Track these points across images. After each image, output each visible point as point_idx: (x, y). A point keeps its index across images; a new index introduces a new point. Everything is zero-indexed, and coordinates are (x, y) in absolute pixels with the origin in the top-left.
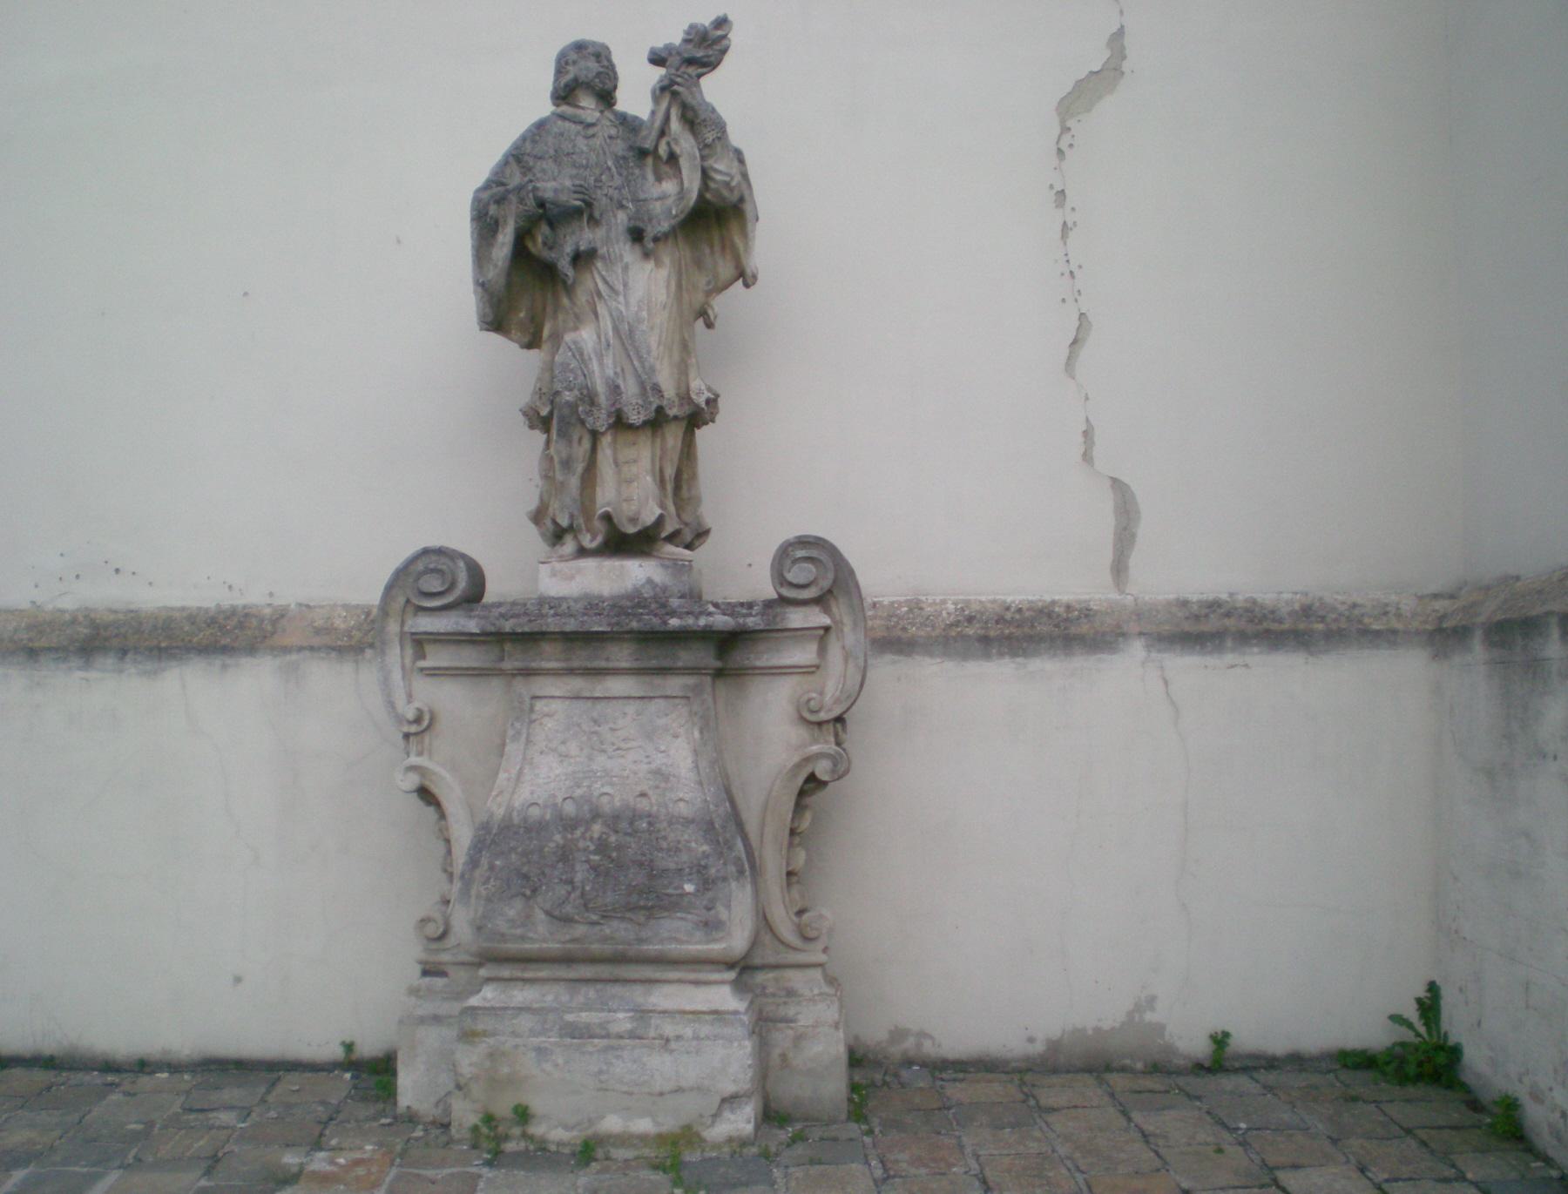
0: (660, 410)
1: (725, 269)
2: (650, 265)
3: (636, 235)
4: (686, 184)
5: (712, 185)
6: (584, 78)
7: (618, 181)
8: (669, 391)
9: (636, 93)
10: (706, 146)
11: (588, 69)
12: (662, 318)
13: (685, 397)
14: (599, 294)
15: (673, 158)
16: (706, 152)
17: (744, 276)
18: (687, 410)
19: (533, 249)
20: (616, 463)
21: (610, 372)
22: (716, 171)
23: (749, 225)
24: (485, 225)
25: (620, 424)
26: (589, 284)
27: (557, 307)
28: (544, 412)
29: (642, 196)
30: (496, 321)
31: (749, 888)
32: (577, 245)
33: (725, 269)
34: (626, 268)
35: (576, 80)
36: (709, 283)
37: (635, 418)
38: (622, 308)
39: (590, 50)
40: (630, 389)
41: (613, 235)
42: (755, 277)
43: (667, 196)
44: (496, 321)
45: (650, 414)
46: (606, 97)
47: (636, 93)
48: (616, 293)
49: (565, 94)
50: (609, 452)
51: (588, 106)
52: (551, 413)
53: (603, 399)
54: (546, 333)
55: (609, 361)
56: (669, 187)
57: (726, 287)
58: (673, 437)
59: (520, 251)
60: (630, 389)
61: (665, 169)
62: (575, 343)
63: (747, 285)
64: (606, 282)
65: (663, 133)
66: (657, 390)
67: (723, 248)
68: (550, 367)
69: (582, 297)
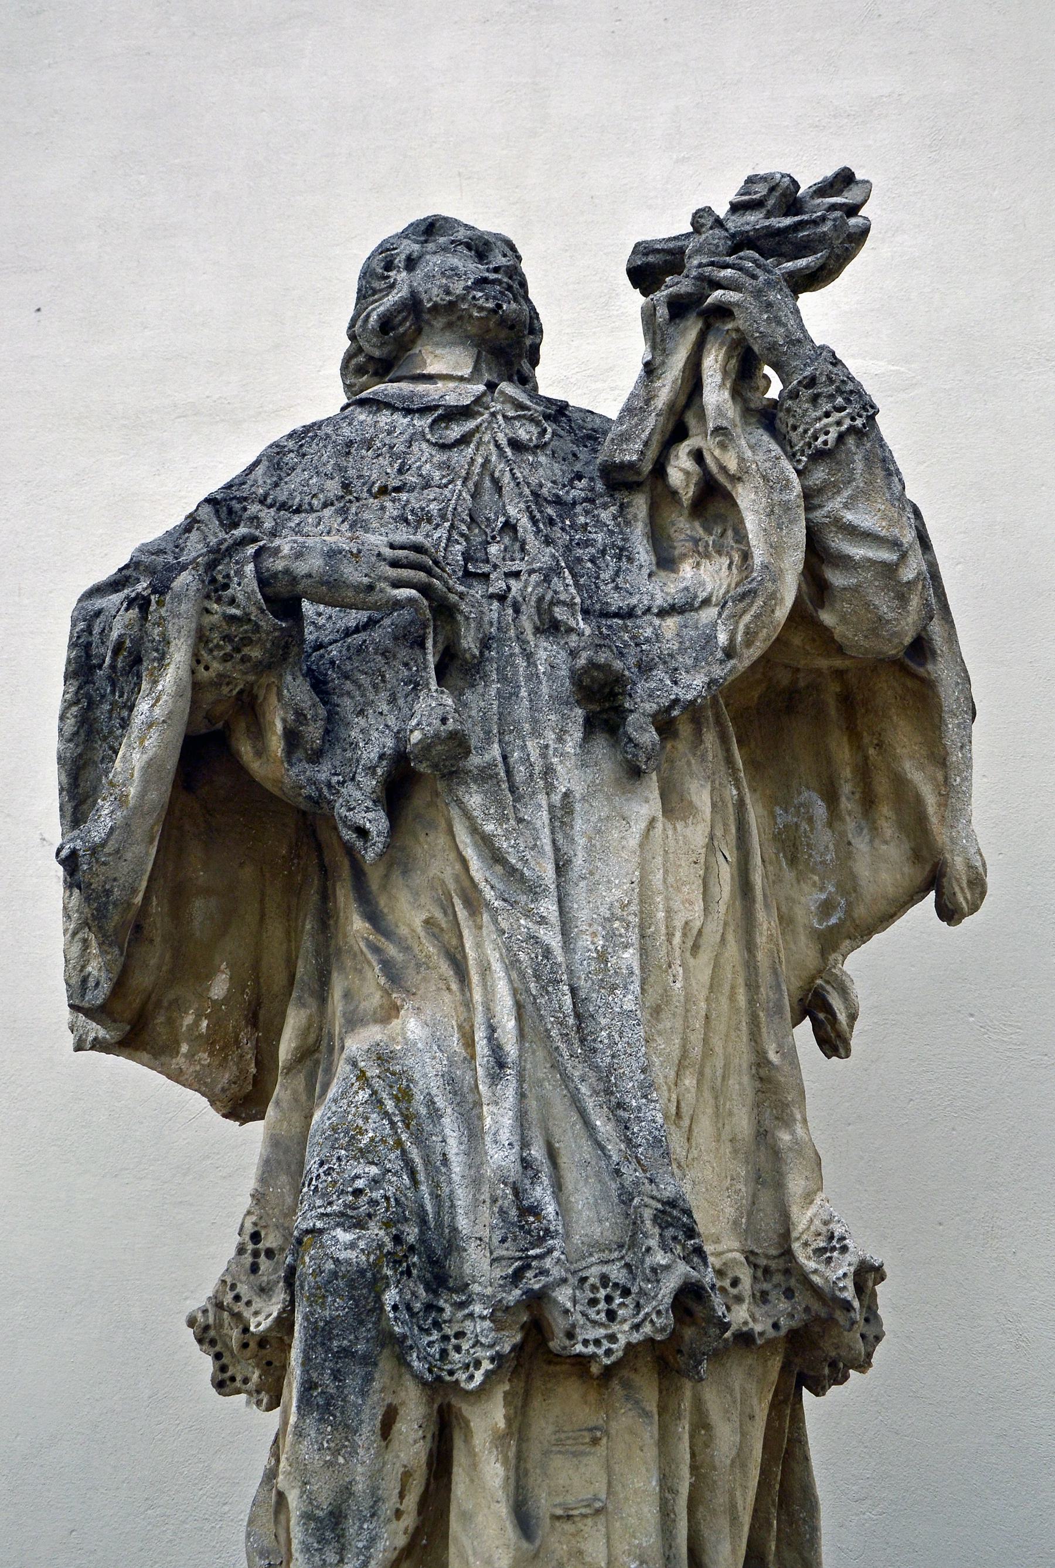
0: (690, 1299)
1: (880, 862)
2: (645, 806)
3: (601, 701)
4: (759, 555)
5: (837, 579)
6: (444, 308)
7: (543, 556)
8: (723, 1244)
9: (595, 354)
10: (820, 455)
11: (454, 273)
12: (689, 979)
13: (776, 1265)
14: (473, 901)
15: (713, 497)
16: (819, 475)
17: (945, 885)
18: (787, 1311)
19: (256, 767)
20: (524, 1520)
21: (500, 1157)
22: (853, 532)
23: (951, 724)
24: (100, 675)
25: (535, 1353)
26: (440, 868)
27: (327, 958)
28: (262, 1318)
29: (616, 602)
30: (125, 1016)
31: (522, 1384)
32: (401, 737)
33: (880, 862)
34: (563, 814)
35: (413, 305)
36: (826, 908)
37: (596, 1334)
38: (552, 938)
39: (461, 235)
40: (584, 1215)
41: (521, 710)
42: (978, 885)
43: (702, 605)
44: (125, 1016)
45: (655, 1316)
46: (510, 342)
47: (595, 354)
48: (534, 890)
49: (380, 352)
50: (493, 1472)
51: (447, 366)
52: (284, 1323)
53: (480, 1266)
54: (286, 1047)
55: (499, 1119)
56: (707, 575)
57: (886, 919)
58: (732, 1410)
59: (205, 752)
60: (584, 1215)
61: (683, 528)
62: (383, 1057)
63: (949, 913)
64: (496, 857)
65: (677, 432)
66: (676, 1220)
67: (868, 802)
68: (285, 1161)
69: (410, 912)
